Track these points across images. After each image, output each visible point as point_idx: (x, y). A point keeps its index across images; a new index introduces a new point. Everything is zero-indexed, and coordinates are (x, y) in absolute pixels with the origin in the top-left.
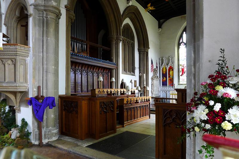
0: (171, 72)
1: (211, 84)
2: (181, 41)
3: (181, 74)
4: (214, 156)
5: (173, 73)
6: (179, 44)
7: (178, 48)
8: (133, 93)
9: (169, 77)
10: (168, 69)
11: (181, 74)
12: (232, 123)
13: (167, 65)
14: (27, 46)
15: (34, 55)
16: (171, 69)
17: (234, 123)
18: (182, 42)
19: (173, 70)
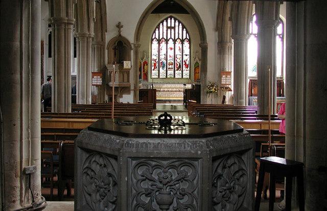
0: (146, 67)
1: (151, 111)
2: (154, 37)
3: (153, 68)
4: (117, 23)
5: (147, 68)
6: (152, 40)
7: (152, 43)
8: (171, 130)
9: (144, 71)
10: (142, 63)
11: (153, 68)
12: (119, 32)
13: (142, 59)
14: (256, 142)
15: (105, 43)
16: (146, 63)
17: (122, 34)
18: (155, 38)
19: (147, 65)
